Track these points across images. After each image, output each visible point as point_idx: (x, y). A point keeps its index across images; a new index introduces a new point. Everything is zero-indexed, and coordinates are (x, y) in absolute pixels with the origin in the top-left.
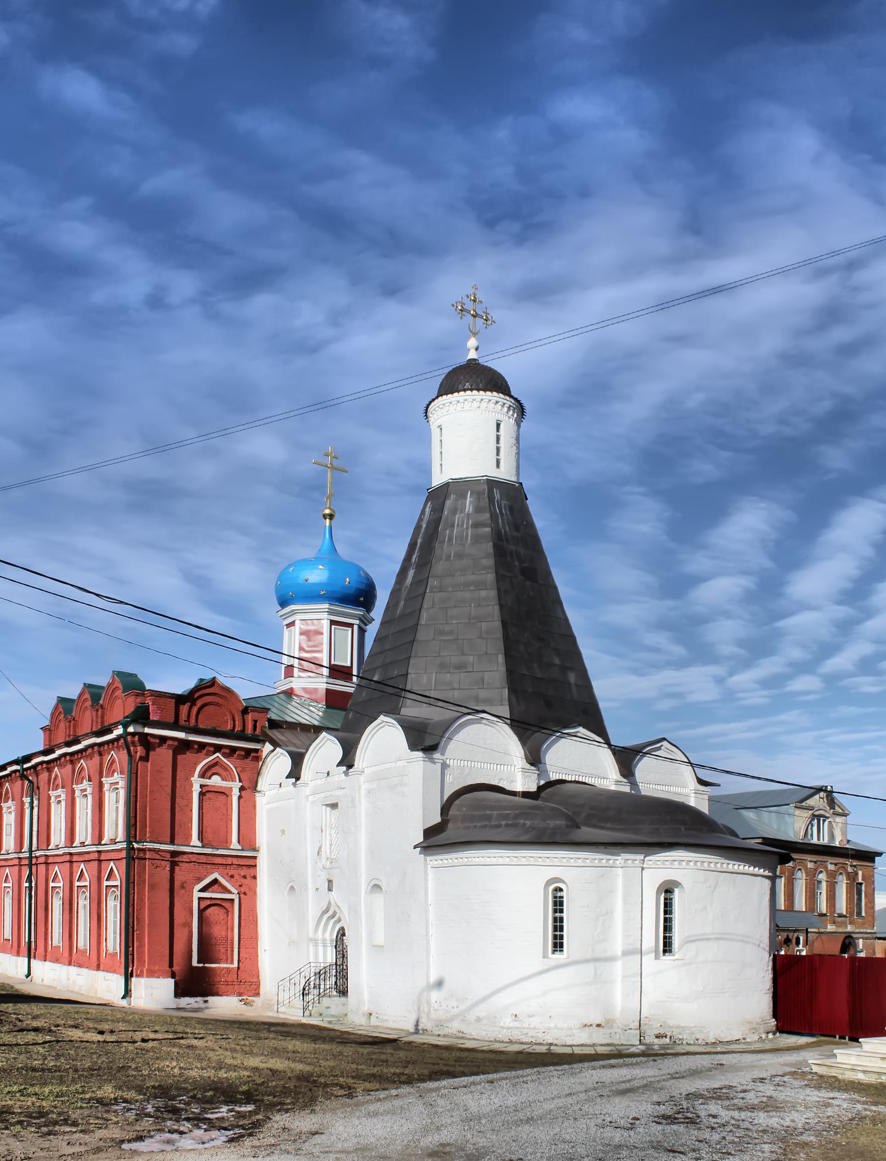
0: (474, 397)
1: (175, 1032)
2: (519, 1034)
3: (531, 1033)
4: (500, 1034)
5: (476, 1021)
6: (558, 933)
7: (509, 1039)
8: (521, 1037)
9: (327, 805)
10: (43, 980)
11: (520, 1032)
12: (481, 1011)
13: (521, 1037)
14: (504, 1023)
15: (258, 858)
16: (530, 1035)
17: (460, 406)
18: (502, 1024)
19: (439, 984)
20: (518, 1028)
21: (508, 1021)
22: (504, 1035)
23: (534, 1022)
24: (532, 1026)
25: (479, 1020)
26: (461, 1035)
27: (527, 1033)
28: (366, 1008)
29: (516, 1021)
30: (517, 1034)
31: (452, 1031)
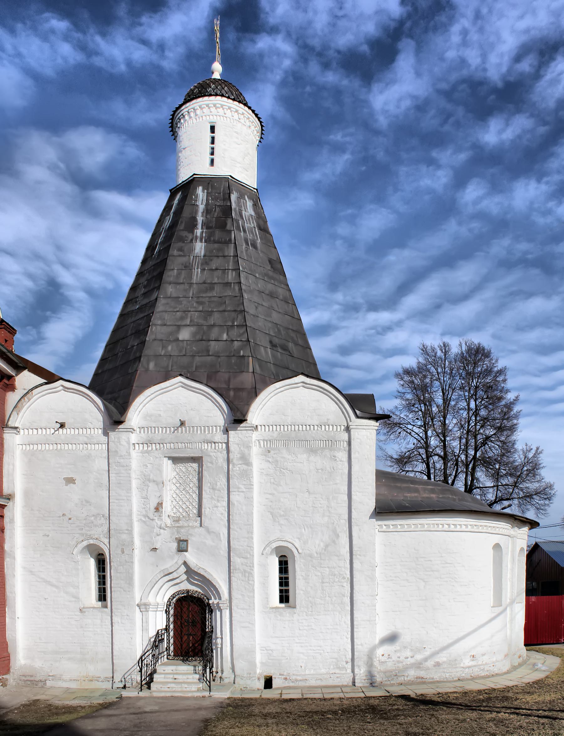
0: (250, 116)
1: (517, 714)
2: (479, 670)
3: (487, 668)
4: (463, 673)
5: (435, 666)
6: (102, 586)
7: (471, 676)
8: (480, 672)
9: (170, 458)
10: (268, 683)
11: (479, 668)
12: (442, 658)
13: (480, 672)
14: (464, 663)
15: (6, 508)
16: (485, 669)
17: (236, 116)
18: (462, 665)
19: (392, 638)
20: (475, 666)
21: (467, 662)
22: (465, 674)
23: (485, 659)
24: (484, 663)
25: (438, 664)
26: (419, 680)
27: (484, 669)
28: (261, 671)
29: (473, 660)
30: (477, 671)
31: (409, 679)
